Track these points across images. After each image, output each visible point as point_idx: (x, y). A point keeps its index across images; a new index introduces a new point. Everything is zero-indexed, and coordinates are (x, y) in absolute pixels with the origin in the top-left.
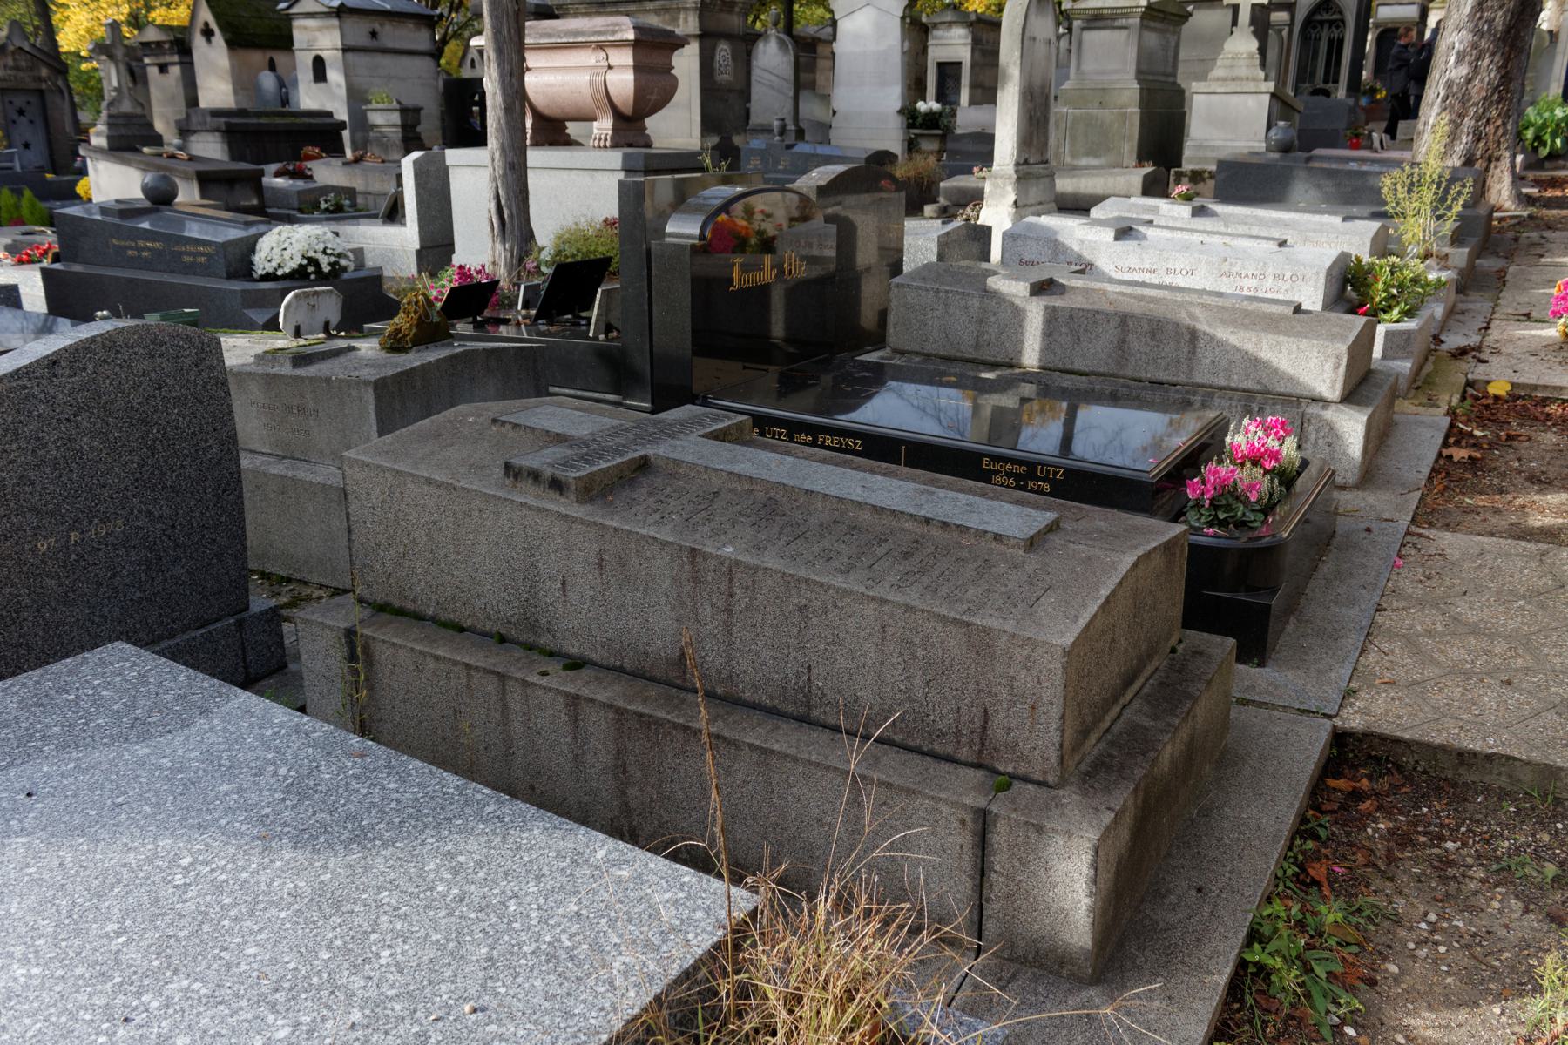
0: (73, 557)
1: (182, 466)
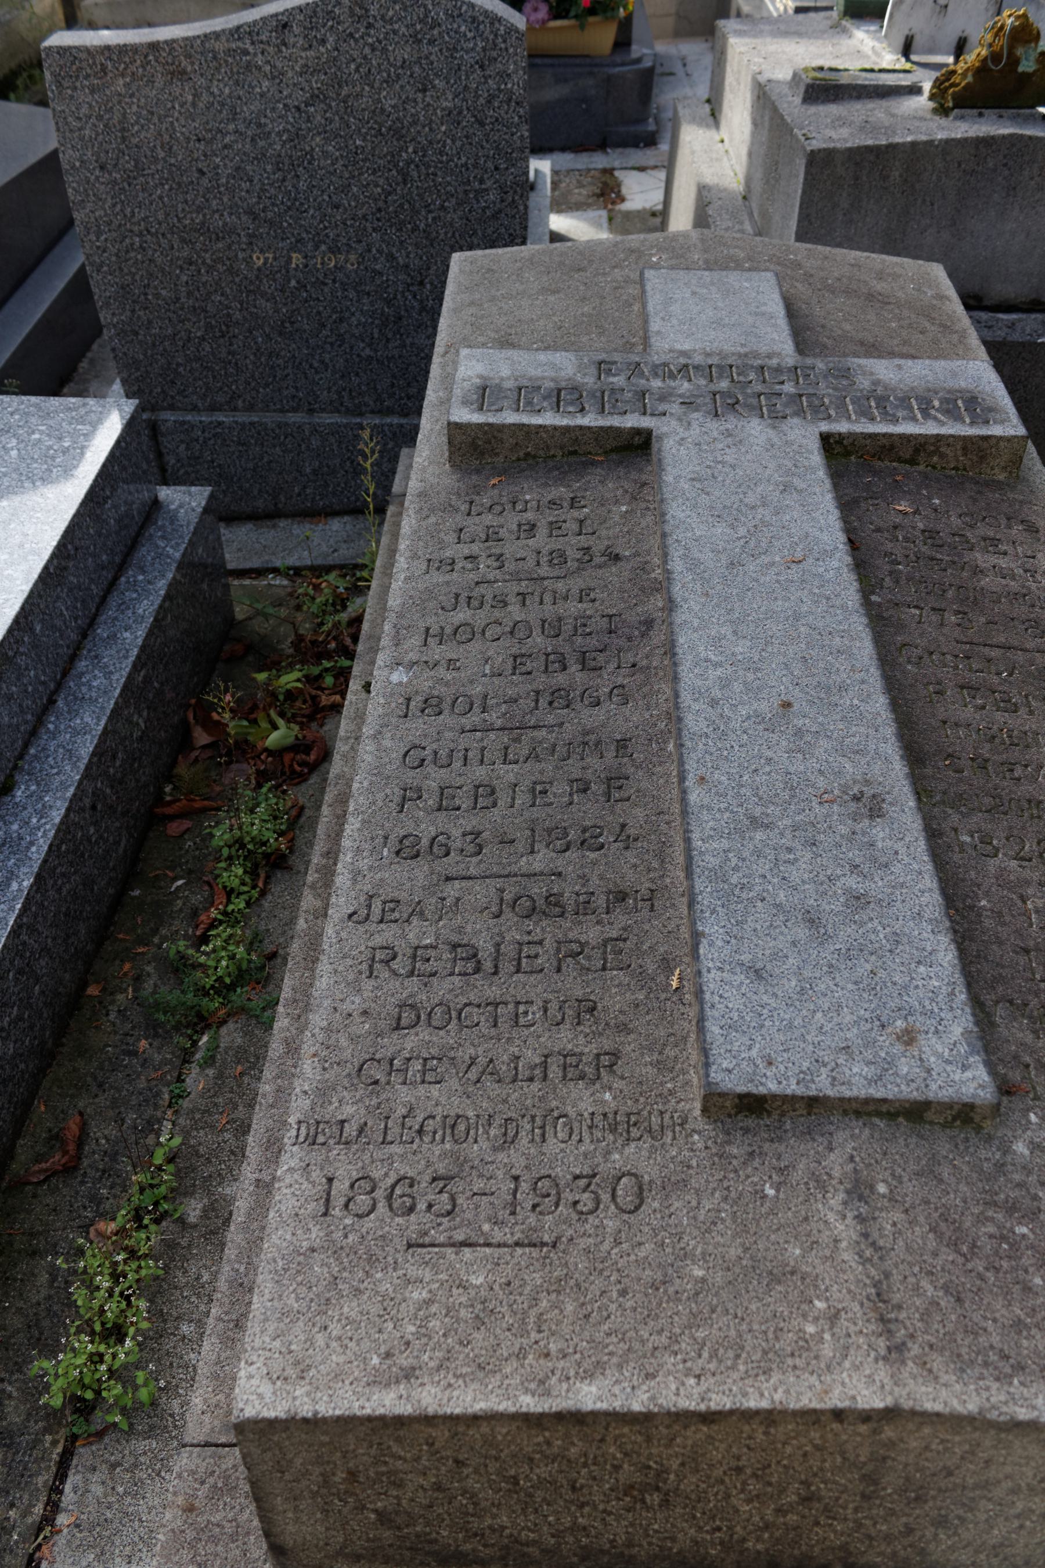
0: (293, 283)
1: (442, 208)
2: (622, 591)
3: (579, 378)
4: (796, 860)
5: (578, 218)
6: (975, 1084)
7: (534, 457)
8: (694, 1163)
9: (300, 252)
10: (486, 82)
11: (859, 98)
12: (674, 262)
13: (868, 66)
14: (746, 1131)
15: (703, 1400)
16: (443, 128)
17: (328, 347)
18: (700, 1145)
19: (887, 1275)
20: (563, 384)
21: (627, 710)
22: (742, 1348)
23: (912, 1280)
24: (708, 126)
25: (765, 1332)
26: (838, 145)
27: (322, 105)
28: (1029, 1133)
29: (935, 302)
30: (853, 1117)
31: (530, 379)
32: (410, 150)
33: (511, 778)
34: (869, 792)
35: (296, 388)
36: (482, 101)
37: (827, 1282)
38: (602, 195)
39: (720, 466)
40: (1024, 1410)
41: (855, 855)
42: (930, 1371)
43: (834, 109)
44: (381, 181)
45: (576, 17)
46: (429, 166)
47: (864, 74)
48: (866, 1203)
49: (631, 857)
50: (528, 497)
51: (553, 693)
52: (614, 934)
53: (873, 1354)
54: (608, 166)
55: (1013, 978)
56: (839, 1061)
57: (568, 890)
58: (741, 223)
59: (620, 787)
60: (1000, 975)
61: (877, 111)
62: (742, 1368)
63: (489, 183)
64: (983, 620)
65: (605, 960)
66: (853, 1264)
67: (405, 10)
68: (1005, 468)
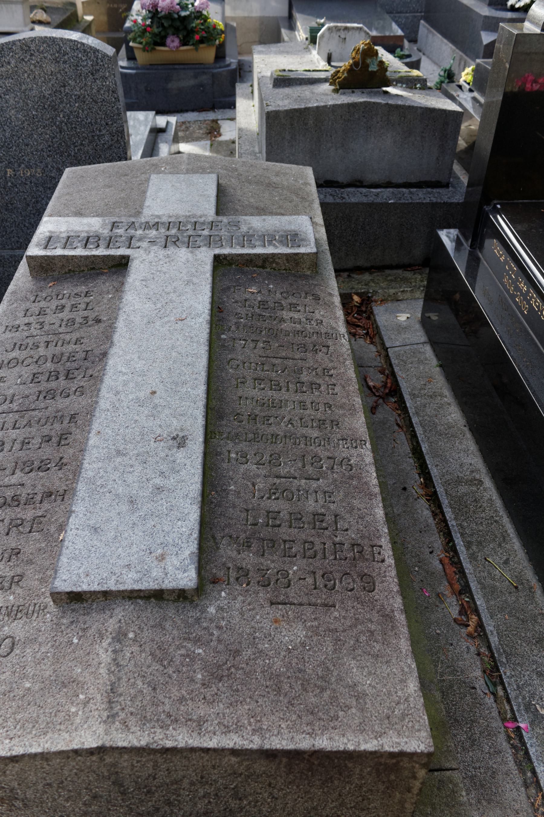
0: (9, 184)
1: (82, 144)
2: (97, 338)
3: (100, 231)
4: (133, 471)
5: (195, 145)
6: (188, 579)
7: (74, 271)
8: (43, 629)
9: (11, 168)
10: (95, 82)
11: (300, 84)
12: (172, 170)
13: (307, 69)
14: (73, 610)
15: (10, 750)
16: (77, 105)
17: (32, 215)
18: (49, 620)
19: (119, 679)
20: (91, 234)
21: (80, 399)
22: (37, 722)
23: (132, 680)
24: (249, 99)
25: (51, 713)
26: (281, 109)
27: (13, 95)
28: (219, 602)
29: (302, 186)
30: (127, 600)
31: (75, 232)
32: (61, 116)
33: (14, 436)
34: (181, 434)
35: (18, 237)
36: (94, 91)
37: (89, 685)
38: (210, 133)
39: (158, 273)
40: (170, 742)
41: (164, 467)
42: (127, 726)
43: (287, 91)
44: (48, 132)
45: (193, 44)
46: (72, 124)
47: (305, 73)
48: (120, 643)
49: (60, 474)
50: (65, 292)
51: (47, 392)
52: (40, 514)
53: (100, 720)
54: (215, 118)
55: (235, 524)
56: (123, 572)
57: (24, 493)
58: (254, 147)
59: (66, 439)
60: (229, 523)
61: (305, 91)
62: (34, 732)
63: (104, 132)
64: (277, 345)
65: (32, 527)
66: (104, 675)
67: (49, 47)
68: (309, 268)
